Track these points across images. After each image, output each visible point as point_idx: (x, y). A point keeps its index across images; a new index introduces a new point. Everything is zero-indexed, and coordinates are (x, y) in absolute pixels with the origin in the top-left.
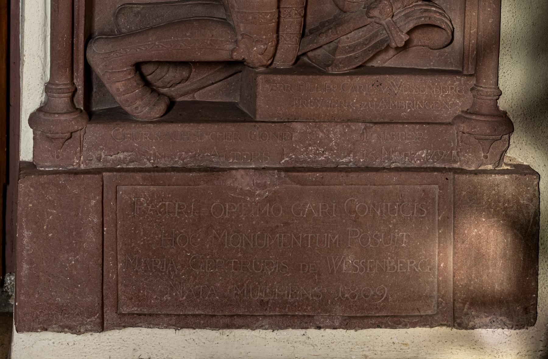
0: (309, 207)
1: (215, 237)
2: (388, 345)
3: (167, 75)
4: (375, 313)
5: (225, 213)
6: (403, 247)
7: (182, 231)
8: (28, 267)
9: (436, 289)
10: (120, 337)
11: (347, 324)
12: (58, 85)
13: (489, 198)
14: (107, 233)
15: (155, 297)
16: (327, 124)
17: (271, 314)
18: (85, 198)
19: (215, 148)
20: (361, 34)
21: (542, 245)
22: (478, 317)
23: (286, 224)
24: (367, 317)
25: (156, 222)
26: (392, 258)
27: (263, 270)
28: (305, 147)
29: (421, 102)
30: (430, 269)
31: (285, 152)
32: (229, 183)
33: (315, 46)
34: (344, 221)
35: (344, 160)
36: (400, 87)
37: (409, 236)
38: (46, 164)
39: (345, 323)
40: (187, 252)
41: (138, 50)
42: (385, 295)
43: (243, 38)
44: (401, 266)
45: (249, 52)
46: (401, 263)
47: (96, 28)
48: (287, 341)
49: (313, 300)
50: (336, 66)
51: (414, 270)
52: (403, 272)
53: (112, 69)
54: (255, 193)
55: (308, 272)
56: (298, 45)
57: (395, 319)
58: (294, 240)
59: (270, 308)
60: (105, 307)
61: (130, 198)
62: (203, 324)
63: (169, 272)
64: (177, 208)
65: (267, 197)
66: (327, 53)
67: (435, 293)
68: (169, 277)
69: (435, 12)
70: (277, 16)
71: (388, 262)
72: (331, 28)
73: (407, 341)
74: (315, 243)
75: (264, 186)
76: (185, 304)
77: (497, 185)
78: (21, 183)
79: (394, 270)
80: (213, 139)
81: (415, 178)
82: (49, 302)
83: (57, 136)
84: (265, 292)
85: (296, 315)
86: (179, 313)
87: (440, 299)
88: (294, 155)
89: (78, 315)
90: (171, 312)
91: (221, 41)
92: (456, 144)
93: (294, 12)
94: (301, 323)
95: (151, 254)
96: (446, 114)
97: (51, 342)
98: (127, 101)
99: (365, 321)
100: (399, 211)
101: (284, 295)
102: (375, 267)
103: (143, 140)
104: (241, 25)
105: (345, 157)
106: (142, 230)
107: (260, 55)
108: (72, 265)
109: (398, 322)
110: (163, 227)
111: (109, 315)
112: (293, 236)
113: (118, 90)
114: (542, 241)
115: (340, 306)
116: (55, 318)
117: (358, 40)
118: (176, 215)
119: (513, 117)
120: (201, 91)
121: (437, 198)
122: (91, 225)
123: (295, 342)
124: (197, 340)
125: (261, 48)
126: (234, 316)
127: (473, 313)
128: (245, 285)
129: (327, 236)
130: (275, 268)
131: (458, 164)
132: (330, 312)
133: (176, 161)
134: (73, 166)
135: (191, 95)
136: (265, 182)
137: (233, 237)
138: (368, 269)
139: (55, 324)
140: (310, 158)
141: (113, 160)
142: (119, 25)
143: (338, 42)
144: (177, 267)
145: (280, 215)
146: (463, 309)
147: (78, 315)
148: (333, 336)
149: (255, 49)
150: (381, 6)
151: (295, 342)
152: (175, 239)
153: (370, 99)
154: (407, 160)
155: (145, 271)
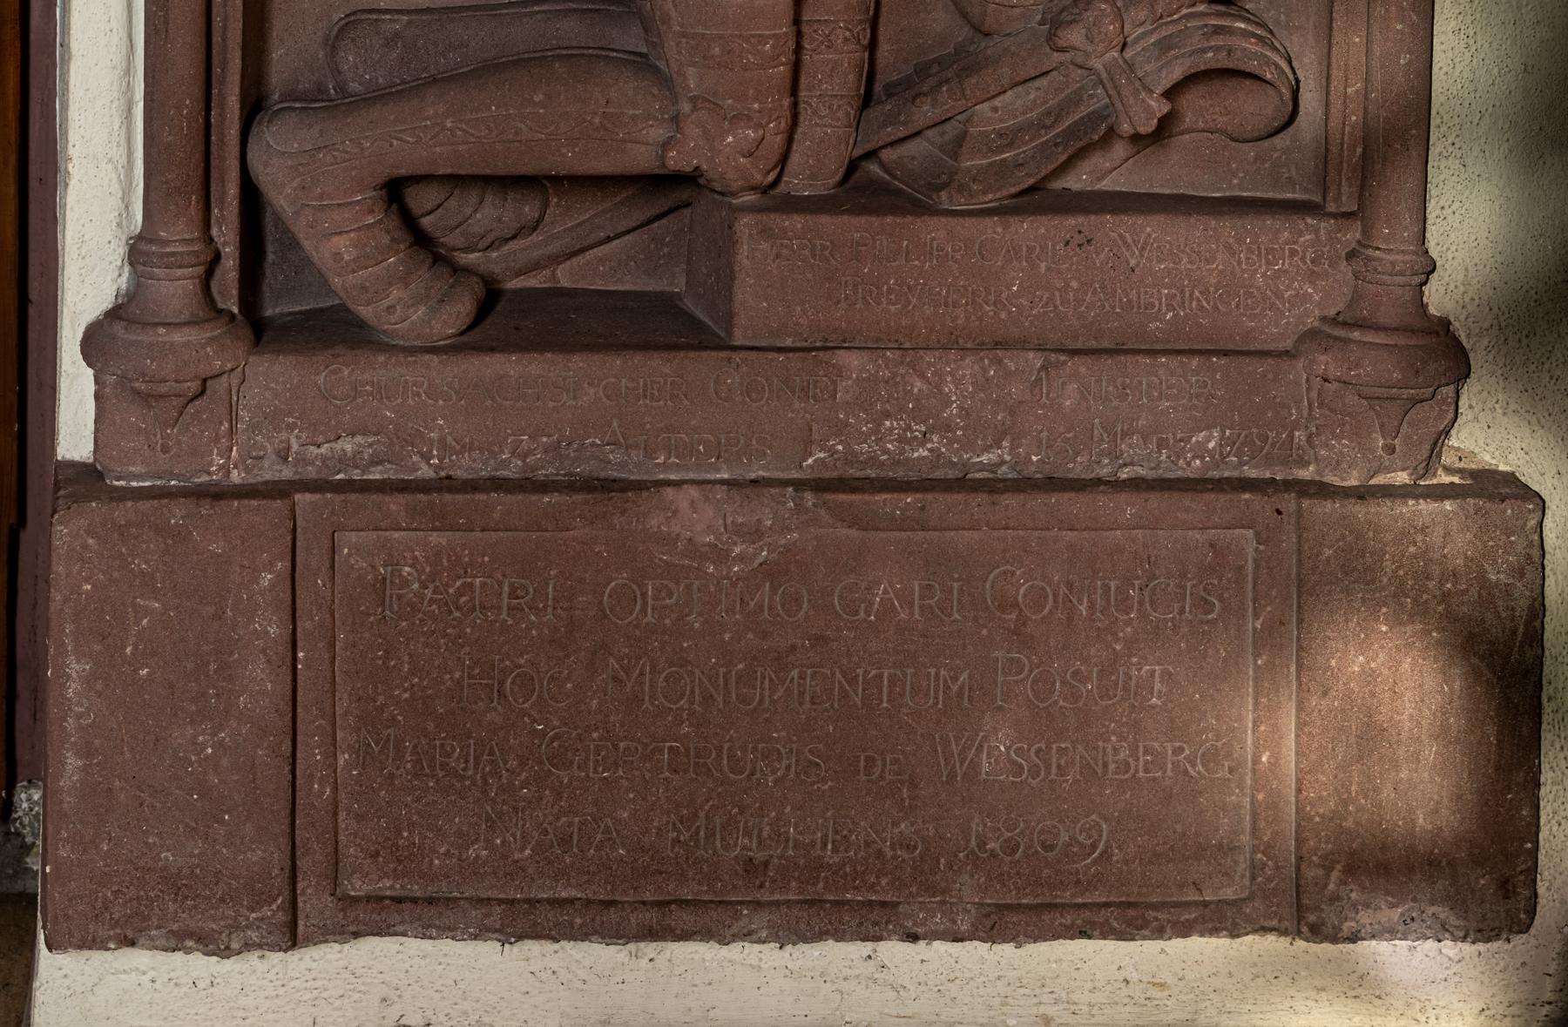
0: (885, 592)
1: (615, 678)
2: (1109, 988)
3: (478, 216)
4: (1073, 896)
5: (644, 611)
6: (1153, 707)
7: (522, 661)
8: (80, 763)
9: (1247, 826)
10: (342, 963)
11: (993, 927)
12: (165, 243)
13: (1398, 568)
14: (307, 667)
15: (443, 850)
16: (937, 353)
17: (777, 897)
18: (243, 567)
19: (615, 424)
20: (1032, 97)
21: (1549, 700)
22: (1367, 906)
23: (819, 640)
24: (1051, 907)
25: (446, 635)
26: (1122, 738)
27: (752, 774)
28: (874, 421)
29: (1205, 292)
30: (1231, 771)
31: (815, 436)
32: (654, 522)
33: (902, 132)
34: (984, 632)
35: (984, 458)
36: (1143, 248)
37: (1170, 674)
38: (132, 469)
39: (989, 924)
40: (534, 721)
41: (395, 143)
42: (1102, 845)
43: (695, 109)
44: (1147, 762)
45: (712, 149)
46: (1146, 752)
47: (274, 81)
48: (822, 975)
49: (895, 857)
50: (961, 189)
51: (1186, 772)
52: (1154, 779)
53: (321, 197)
54: (729, 551)
55: (882, 777)
56: (853, 129)
57: (1131, 913)
58: (841, 687)
59: (774, 881)
60: (300, 878)
61: (373, 567)
62: (581, 926)
63: (484, 779)
64: (505, 595)
65: (765, 562)
66: (936, 151)
67: (1245, 838)
68: (485, 792)
69: (1245, 34)
70: (791, 45)
71: (1109, 750)
72: (947, 81)
73: (1166, 976)
74: (902, 695)
75: (754, 534)
76: (530, 871)
77: (1423, 529)
78: (61, 523)
79: (1127, 772)
80: (608, 397)
81: (1187, 510)
82: (142, 863)
83: (163, 389)
84: (759, 835)
85: (848, 902)
86: (511, 894)
87: (1259, 856)
88: (841, 442)
89: (222, 900)
90: (490, 894)
91: (634, 117)
92: (1305, 413)
93: (842, 34)
94: (861, 924)
95: (431, 726)
96: (1277, 325)
97: (145, 979)
98: (364, 288)
99: (1046, 917)
100: (1141, 603)
101: (813, 844)
102: (1073, 763)
103: (410, 401)
104: (691, 71)
105: (987, 449)
106: (406, 658)
107: (744, 157)
108: (207, 758)
109: (1140, 922)
110: (467, 649)
111: (313, 900)
112: (838, 675)
113: (337, 256)
114: (1551, 689)
115: (972, 876)
116: (157, 911)
117: (1023, 113)
118: (504, 616)
119: (1468, 336)
120: (574, 260)
121: (1250, 566)
122: (260, 643)
123: (845, 979)
124: (562, 973)
125: (746, 137)
126: (669, 903)
127: (1353, 895)
128: (702, 814)
129: (937, 674)
130: (788, 768)
131: (1311, 468)
132: (943, 892)
133: (503, 461)
134: (209, 473)
135: (547, 272)
136: (759, 521)
137: (666, 679)
138: (1054, 770)
139: (159, 927)
140: (886, 451)
141: (324, 459)
142: (339, 73)
143: (968, 120)
144: (506, 763)
145: (802, 614)
146: (1326, 885)
147: (222, 900)
148: (952, 961)
149: (730, 139)
150: (1090, 16)
151: (845, 979)
152: (501, 683)
153: (1059, 284)
154: (1163, 457)
155: (416, 776)
